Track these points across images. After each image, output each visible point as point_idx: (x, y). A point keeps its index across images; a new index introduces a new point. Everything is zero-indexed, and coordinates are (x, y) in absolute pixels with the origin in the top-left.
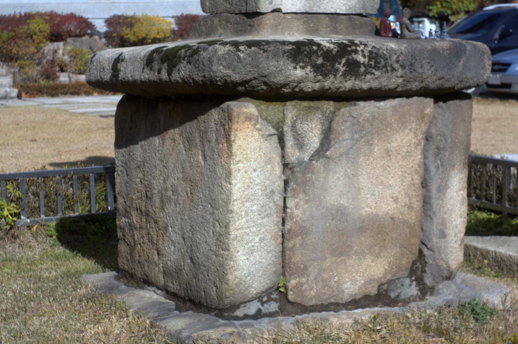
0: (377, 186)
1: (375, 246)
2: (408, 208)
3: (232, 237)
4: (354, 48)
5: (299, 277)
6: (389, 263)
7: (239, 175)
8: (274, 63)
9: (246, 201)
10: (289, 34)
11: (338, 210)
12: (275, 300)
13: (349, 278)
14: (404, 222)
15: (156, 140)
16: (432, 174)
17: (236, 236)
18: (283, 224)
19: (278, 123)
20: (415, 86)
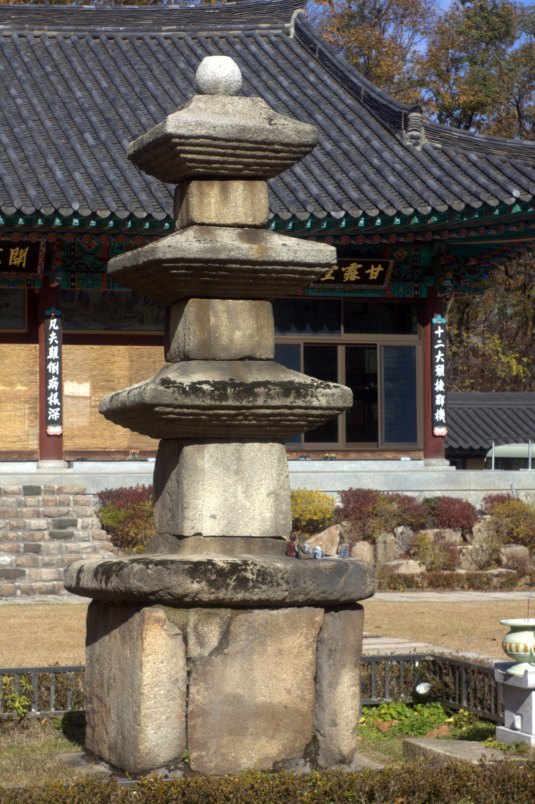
0: (271, 679)
1: (270, 729)
2: (301, 699)
3: (142, 714)
4: (244, 567)
5: (200, 751)
6: (283, 745)
7: (148, 665)
9: (155, 686)
10: (207, 554)
11: (234, 697)
12: (181, 769)
13: (245, 755)
14: (297, 711)
15: (107, 638)
16: (325, 671)
17: (146, 714)
18: (187, 706)
19: (183, 625)
20: (301, 598)
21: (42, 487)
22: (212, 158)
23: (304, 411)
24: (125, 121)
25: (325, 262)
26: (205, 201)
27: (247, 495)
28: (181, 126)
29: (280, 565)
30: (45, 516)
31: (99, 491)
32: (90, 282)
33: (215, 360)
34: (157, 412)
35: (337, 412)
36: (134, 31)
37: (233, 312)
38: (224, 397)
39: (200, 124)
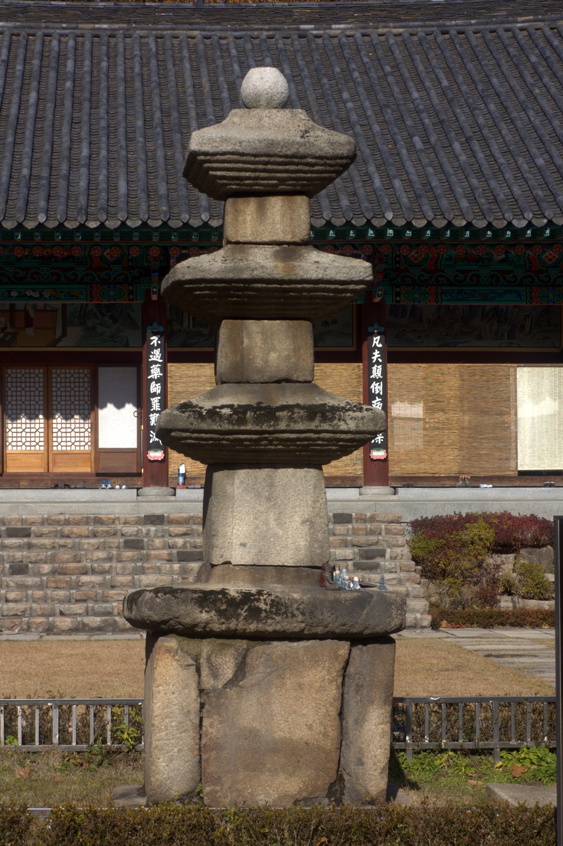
1: (289, 766)
2: (323, 735)
4: (257, 597)
6: (304, 783)
8: (183, 607)
9: (166, 718)
11: (251, 732)
17: (157, 747)
18: (200, 739)
19: (197, 656)
20: (320, 630)
21: (354, 515)
22: (243, 174)
23: (332, 435)
24: (461, 122)
25: (358, 279)
26: (241, 219)
27: (280, 523)
28: (205, 143)
29: (296, 596)
30: (353, 546)
31: (413, 519)
32: (416, 296)
33: (248, 382)
34: (173, 436)
35: (369, 436)
36: (487, 23)
37: (268, 333)
38: (242, 421)
39: (225, 140)
